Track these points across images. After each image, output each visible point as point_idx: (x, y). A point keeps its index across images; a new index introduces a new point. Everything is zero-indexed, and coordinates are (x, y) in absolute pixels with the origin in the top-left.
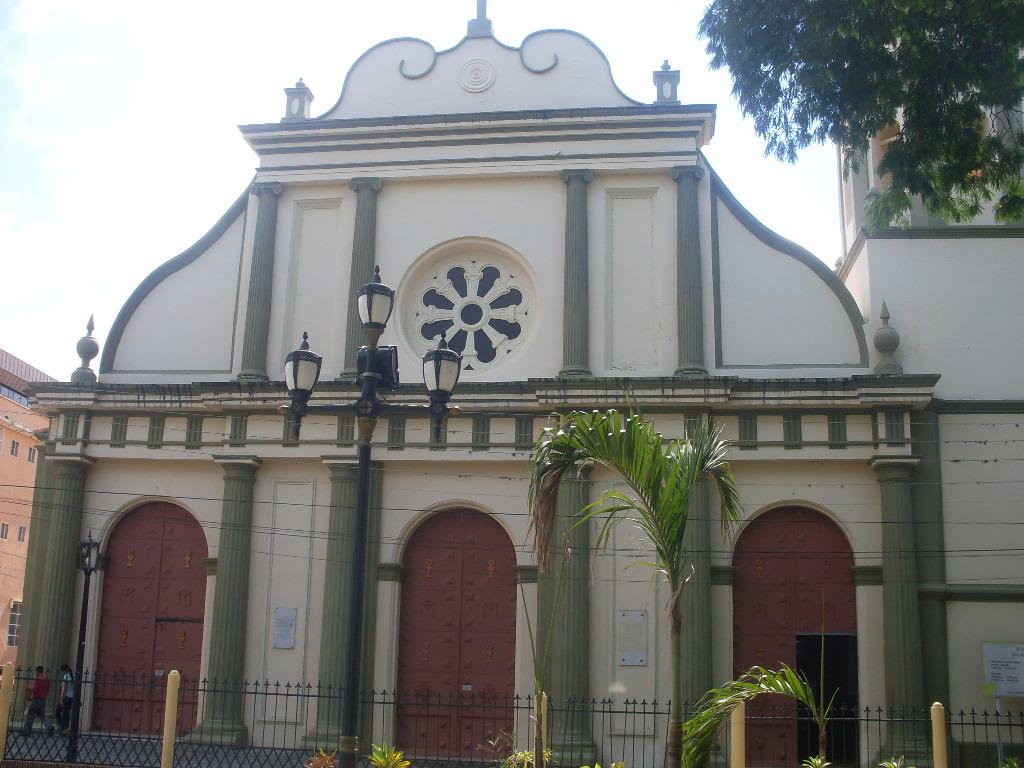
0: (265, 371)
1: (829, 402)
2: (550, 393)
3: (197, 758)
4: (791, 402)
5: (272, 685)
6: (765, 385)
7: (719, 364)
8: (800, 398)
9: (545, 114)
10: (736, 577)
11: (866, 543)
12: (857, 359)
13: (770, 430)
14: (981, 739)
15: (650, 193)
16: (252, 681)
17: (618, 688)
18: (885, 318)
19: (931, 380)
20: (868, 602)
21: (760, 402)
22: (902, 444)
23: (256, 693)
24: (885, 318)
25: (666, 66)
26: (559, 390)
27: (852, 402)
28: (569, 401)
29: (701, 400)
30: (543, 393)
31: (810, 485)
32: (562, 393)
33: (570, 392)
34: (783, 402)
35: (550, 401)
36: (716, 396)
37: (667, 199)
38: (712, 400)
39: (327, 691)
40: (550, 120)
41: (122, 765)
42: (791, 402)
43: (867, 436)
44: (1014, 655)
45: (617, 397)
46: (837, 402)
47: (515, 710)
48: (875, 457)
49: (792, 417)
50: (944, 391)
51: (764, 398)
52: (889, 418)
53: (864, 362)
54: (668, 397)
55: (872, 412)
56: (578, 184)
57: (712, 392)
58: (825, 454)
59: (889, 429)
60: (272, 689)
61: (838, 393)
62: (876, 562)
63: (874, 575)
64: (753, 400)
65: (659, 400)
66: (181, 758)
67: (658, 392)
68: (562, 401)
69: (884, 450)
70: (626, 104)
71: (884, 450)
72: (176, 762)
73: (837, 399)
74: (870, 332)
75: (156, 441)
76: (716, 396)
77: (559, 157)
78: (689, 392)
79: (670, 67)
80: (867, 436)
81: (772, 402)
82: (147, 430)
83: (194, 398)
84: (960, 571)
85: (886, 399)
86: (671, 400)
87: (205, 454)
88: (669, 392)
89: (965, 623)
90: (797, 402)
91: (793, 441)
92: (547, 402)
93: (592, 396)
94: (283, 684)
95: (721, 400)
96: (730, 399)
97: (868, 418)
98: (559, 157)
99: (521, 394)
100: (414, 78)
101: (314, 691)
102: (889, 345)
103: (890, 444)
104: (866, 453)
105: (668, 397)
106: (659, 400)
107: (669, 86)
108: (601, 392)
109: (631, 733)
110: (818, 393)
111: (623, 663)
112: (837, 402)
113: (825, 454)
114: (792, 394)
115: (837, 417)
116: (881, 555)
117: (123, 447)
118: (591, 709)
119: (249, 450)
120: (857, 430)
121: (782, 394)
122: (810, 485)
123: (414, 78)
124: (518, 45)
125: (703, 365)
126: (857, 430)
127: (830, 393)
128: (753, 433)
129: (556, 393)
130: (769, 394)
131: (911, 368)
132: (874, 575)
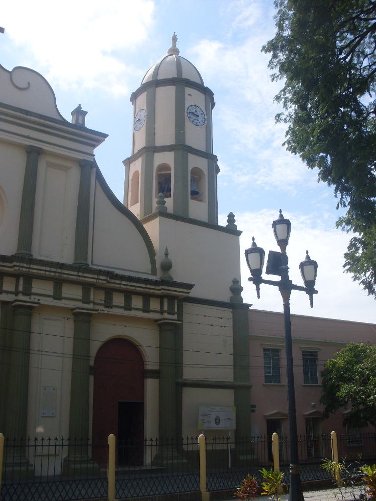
0: (30, 251)
1: (147, 290)
2: (22, 265)
3: (52, 491)
4: (132, 288)
5: (185, 439)
6: (122, 278)
7: (92, 264)
8: (136, 287)
9: (27, 113)
10: (93, 370)
11: (151, 359)
12: (150, 272)
13: (118, 300)
14: (221, 448)
15: (66, 169)
16: (148, 439)
17: (40, 430)
18: (167, 254)
19: (190, 286)
20: (151, 386)
21: (118, 286)
22: (173, 314)
23: (49, 446)
24: (167, 254)
25: (79, 107)
26: (27, 264)
27: (157, 292)
28: (31, 270)
29: (95, 281)
30: (18, 264)
31: (125, 326)
32: (28, 266)
33: (32, 266)
34: (128, 287)
35: (21, 269)
36: (102, 280)
37: (75, 174)
38: (100, 281)
39: (155, 442)
40: (29, 117)
41: (83, 498)
42: (132, 288)
43: (13, 289)
44: (210, 411)
45: (55, 272)
46: (151, 291)
47: (145, 447)
48: (16, 301)
49: (128, 295)
50: (194, 293)
51: (121, 284)
52: (169, 300)
53: (154, 272)
54: (80, 276)
55: (161, 297)
56: (33, 154)
57: (101, 277)
58: (121, 312)
59: (24, 287)
60: (39, 443)
61: (152, 287)
62: (156, 368)
63: (155, 374)
64: (116, 284)
65: (75, 277)
66: (62, 491)
67: (76, 273)
68: (27, 270)
69: (166, 315)
70: (57, 118)
71: (166, 315)
72: (106, 490)
73: (151, 289)
74: (159, 259)
75: (128, 307)
76: (102, 280)
77: (28, 137)
78: (91, 276)
79: (81, 108)
80: (13, 289)
81: (124, 287)
82: (52, 289)
83: (157, 288)
84: (189, 374)
85: (172, 293)
86: (81, 278)
87: (133, 313)
88: (81, 274)
89: (190, 396)
90: (134, 288)
91: (128, 307)
92: (19, 269)
93: (44, 270)
94: (53, 438)
95: (104, 282)
96: (108, 282)
97: (14, 279)
98: (28, 137)
99: (3, 262)
100: (11, 80)
101: (66, 443)
102: (167, 267)
103: (169, 313)
104: (157, 316)
105: (80, 276)
106: (75, 277)
107: (79, 121)
108: (48, 269)
109: (47, 453)
110: (143, 286)
111: (43, 416)
112: (151, 291)
113: (121, 312)
114: (133, 284)
115: (147, 297)
116: (71, 356)
117: (112, 308)
118: (27, 444)
119: (34, 298)
120: (154, 305)
121: (129, 283)
122: (125, 326)
123: (11, 80)
124: (10, 70)
125: (30, 251)
126: (154, 305)
127: (148, 286)
128: (30, 288)
129: (25, 265)
130: (123, 282)
131: (177, 279)
132: (155, 374)
